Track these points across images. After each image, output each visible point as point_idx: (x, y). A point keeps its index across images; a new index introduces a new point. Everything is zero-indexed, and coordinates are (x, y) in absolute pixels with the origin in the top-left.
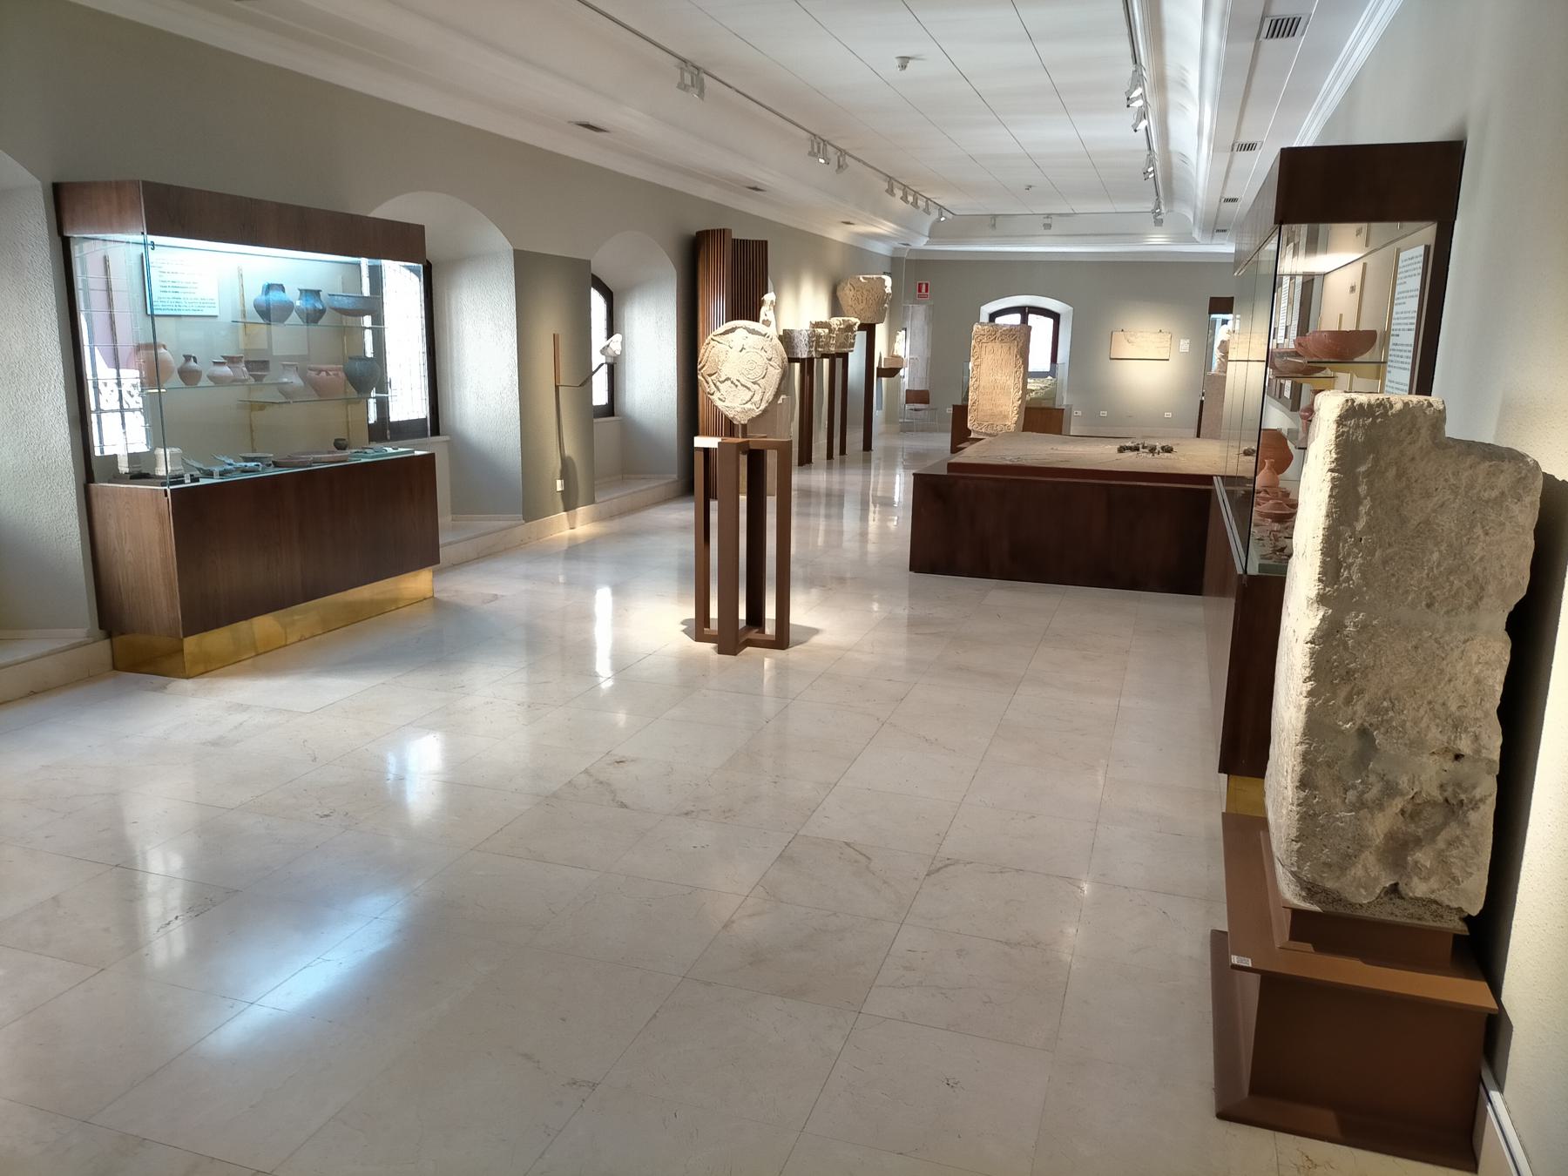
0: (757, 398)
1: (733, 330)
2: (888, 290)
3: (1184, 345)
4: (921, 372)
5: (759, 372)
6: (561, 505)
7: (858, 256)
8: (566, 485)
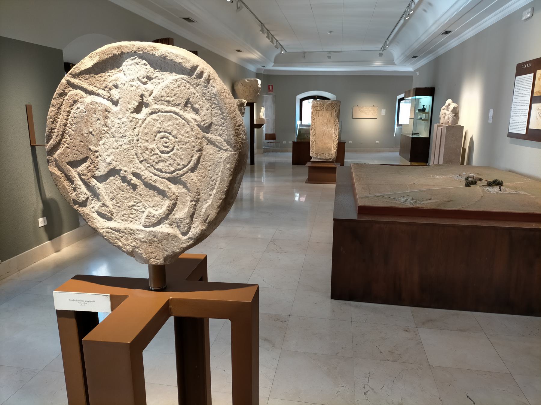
0: (181, 213)
1: (113, 62)
2: (259, 86)
3: (383, 112)
4: (271, 126)
5: (182, 157)
6: (44, 235)
7: (242, 71)
8: (49, 221)
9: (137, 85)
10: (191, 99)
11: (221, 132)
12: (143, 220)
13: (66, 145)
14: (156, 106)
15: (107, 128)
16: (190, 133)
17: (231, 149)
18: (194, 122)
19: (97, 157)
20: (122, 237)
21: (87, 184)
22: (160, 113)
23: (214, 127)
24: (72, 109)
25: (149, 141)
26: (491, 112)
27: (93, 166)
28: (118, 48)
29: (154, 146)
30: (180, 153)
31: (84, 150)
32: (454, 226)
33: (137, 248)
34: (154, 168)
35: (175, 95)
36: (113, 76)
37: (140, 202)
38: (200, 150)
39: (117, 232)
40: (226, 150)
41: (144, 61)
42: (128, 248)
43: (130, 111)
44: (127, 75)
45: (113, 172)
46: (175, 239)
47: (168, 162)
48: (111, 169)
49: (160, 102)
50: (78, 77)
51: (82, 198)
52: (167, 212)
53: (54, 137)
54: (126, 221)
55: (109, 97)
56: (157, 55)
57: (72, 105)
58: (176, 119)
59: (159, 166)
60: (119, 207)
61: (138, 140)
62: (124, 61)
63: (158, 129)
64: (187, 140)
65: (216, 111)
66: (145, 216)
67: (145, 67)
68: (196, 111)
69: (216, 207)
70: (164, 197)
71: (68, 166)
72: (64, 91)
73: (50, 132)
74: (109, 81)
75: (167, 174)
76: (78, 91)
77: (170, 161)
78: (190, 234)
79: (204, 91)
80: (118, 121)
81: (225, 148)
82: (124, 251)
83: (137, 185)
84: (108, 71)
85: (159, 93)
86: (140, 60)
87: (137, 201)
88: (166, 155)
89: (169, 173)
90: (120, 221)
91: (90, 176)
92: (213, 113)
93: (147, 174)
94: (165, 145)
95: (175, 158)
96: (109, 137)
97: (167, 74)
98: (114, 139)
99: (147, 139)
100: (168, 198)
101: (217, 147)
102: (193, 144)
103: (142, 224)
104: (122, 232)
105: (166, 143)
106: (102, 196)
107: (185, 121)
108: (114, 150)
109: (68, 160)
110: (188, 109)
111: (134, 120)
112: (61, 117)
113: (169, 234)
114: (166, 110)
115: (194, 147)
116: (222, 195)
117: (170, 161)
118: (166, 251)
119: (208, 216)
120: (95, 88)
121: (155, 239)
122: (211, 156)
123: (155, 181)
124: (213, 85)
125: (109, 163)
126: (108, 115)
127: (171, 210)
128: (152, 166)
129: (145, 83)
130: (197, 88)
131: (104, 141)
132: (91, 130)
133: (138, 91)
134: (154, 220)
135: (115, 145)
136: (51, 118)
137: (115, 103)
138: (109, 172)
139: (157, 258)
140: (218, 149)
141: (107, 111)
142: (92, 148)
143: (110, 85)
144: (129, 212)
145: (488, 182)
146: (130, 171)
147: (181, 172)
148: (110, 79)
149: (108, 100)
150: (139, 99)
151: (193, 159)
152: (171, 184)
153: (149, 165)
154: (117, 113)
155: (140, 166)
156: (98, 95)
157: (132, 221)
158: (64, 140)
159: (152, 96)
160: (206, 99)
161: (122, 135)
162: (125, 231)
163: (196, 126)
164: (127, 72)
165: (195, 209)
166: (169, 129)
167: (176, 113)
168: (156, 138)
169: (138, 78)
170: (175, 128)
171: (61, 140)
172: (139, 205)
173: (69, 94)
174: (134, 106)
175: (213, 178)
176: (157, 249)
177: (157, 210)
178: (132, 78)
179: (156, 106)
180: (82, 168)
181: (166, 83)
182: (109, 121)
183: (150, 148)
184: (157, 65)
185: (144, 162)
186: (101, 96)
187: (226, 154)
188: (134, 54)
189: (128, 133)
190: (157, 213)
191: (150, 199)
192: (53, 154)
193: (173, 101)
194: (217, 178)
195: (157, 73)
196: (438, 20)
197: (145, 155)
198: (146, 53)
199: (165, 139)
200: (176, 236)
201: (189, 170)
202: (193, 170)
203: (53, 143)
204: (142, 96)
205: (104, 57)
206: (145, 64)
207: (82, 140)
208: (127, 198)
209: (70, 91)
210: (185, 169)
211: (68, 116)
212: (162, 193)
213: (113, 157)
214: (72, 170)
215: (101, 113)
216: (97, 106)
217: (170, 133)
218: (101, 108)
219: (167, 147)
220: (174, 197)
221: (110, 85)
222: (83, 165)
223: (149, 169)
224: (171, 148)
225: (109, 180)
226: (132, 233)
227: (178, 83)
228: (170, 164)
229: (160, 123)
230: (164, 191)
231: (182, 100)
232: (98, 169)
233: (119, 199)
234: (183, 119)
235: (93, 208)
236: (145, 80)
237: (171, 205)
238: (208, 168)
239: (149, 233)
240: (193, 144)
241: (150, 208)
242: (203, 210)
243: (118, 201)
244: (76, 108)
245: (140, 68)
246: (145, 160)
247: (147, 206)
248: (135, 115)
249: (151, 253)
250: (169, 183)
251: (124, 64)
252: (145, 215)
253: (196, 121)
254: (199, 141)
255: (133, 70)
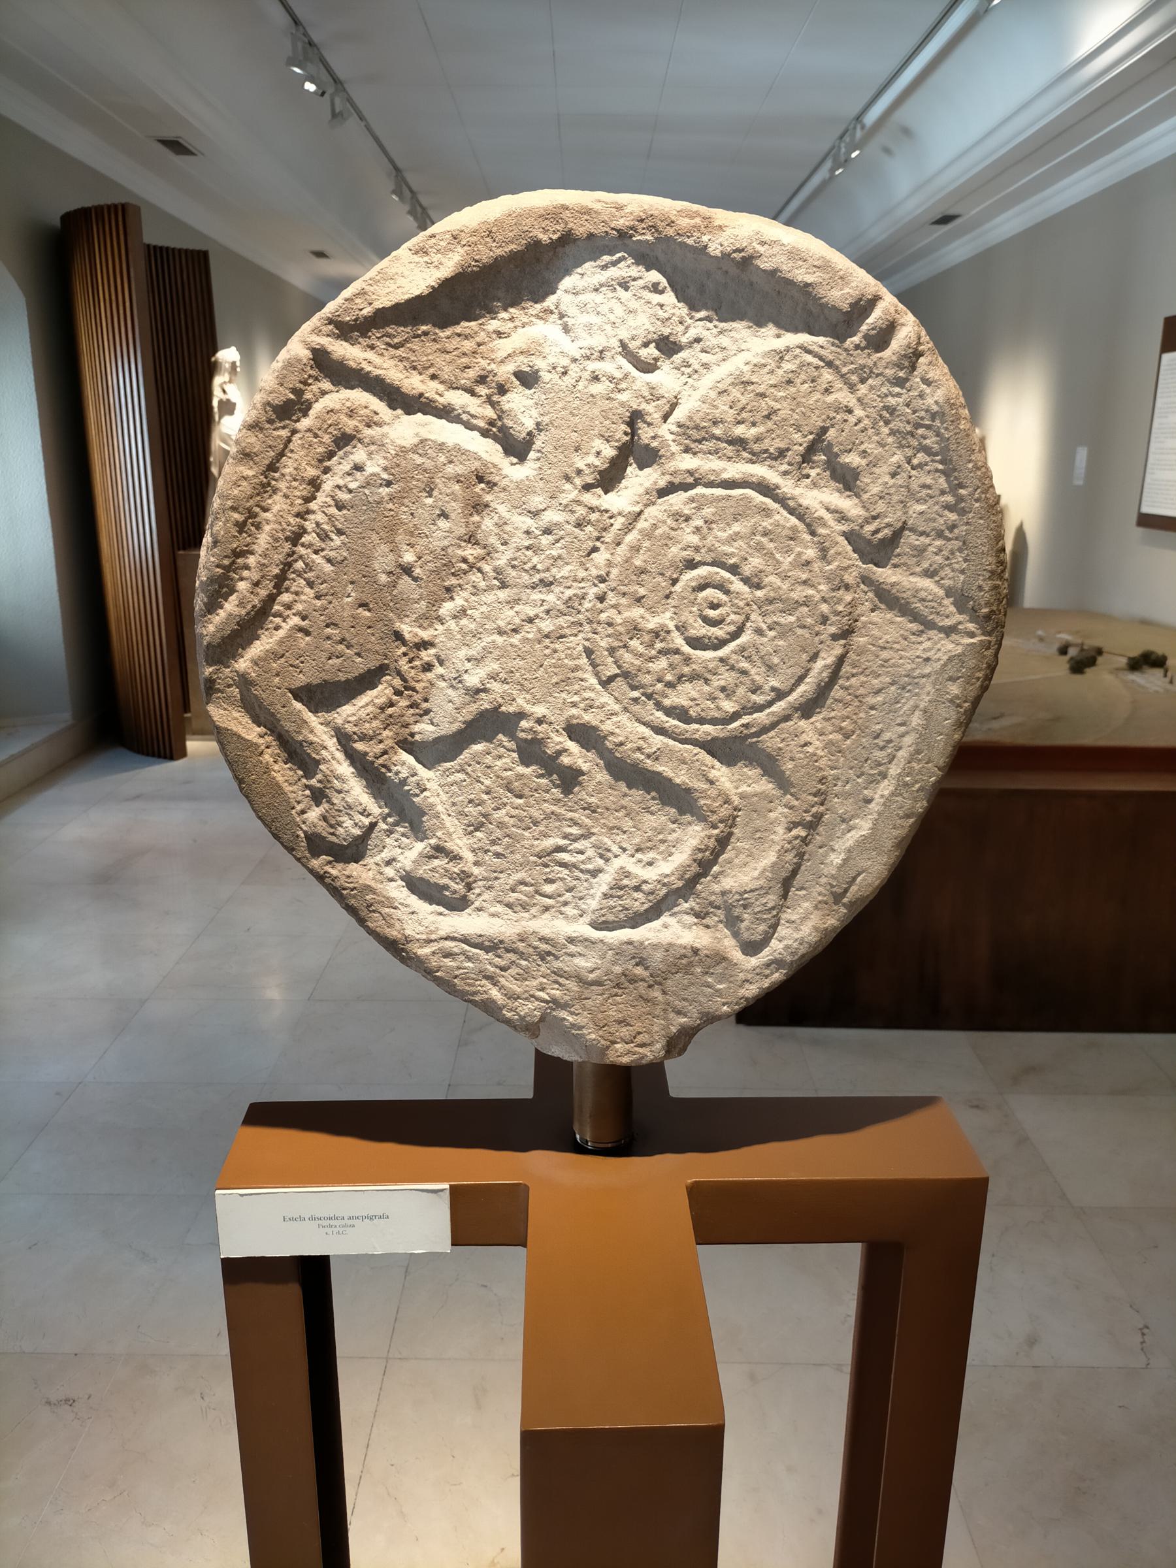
0: (744, 872)
1: (520, 274)
5: (769, 657)
9: (618, 375)
10: (832, 433)
11: (939, 559)
12: (593, 904)
13: (296, 620)
14: (688, 462)
15: (478, 551)
16: (816, 566)
17: (971, 626)
18: (832, 523)
19: (428, 667)
20: (503, 969)
21: (373, 775)
22: (700, 490)
23: (910, 538)
24: (326, 470)
25: (648, 602)
26: (1082, 454)
27: (404, 703)
28: (553, 214)
29: (666, 619)
30: (766, 643)
31: (372, 640)
32: (1091, 795)
33: (565, 1006)
34: (659, 706)
35: (768, 417)
36: (514, 334)
37: (587, 835)
38: (846, 633)
39: (487, 950)
40: (949, 631)
41: (654, 276)
42: (529, 1009)
43: (578, 481)
44: (580, 331)
45: (490, 724)
46: (718, 970)
47: (717, 682)
48: (483, 714)
49: (709, 445)
50: (364, 335)
51: (350, 827)
52: (695, 868)
53: (242, 586)
54: (525, 907)
55: (492, 423)
56: (714, 250)
57: (331, 455)
58: (766, 512)
59: (673, 699)
60: (498, 855)
61: (601, 599)
62: (568, 272)
63: (689, 553)
64: (799, 593)
65: (928, 480)
66: (605, 888)
67: (656, 298)
68: (846, 479)
69: (889, 844)
70: (682, 812)
71: (298, 706)
72: (298, 393)
73: (228, 569)
74: (502, 354)
75: (708, 728)
76: (359, 397)
77: (726, 678)
78: (776, 947)
79: (892, 401)
80: (528, 522)
81: (948, 622)
82: (507, 1021)
83: (581, 773)
84: (492, 313)
85: (705, 408)
86: (635, 271)
87: (575, 831)
88: (709, 654)
89: (713, 722)
90: (499, 908)
91: (390, 742)
92: (914, 486)
93: (627, 730)
94: (712, 613)
95: (745, 665)
96: (482, 584)
97: (740, 329)
98: (503, 595)
99: (642, 591)
100: (702, 818)
101: (915, 617)
102: (824, 608)
103: (587, 919)
104: (508, 951)
105: (714, 606)
106: (437, 816)
107: (801, 518)
108: (500, 640)
109: (301, 680)
110: (813, 473)
111: (594, 517)
112: (277, 503)
113: (696, 951)
114: (725, 476)
115: (824, 620)
116: (915, 800)
117: (726, 678)
118: (679, 1013)
119: (854, 879)
120: (434, 385)
121: (639, 971)
122: (885, 655)
123: (656, 757)
124: (930, 375)
125: (478, 691)
126: (488, 498)
127: (705, 864)
128: (649, 697)
129: (647, 367)
130: (863, 389)
131: (459, 601)
132: (409, 557)
133: (623, 397)
134: (639, 902)
135: (509, 615)
136: (234, 509)
137: (517, 448)
138: (469, 724)
139: (640, 1039)
140: (915, 627)
141: (480, 479)
142: (407, 629)
143: (505, 371)
144: (539, 872)
145: (1130, 659)
146: (559, 720)
147: (761, 717)
148: (503, 347)
149: (485, 433)
150: (620, 432)
151: (819, 664)
152: (717, 764)
153: (636, 694)
154: (525, 488)
155: (605, 698)
156: (446, 413)
157: (546, 909)
158: (286, 597)
159: (671, 420)
160: (892, 433)
161: (536, 578)
162: (521, 946)
163: (841, 539)
164: (578, 319)
165: (801, 855)
166: (733, 551)
167: (765, 489)
168: (678, 588)
169: (623, 345)
170: (759, 548)
171: (271, 599)
172: (578, 845)
173: (317, 408)
174: (597, 462)
175: (887, 736)
176: (642, 1008)
177: (650, 864)
178: (598, 341)
179: (688, 462)
180: (348, 713)
181: (737, 364)
182: (488, 523)
183: (650, 626)
184: (702, 290)
185: (620, 684)
186: (457, 420)
187: (950, 646)
188: (618, 242)
189: (566, 571)
190: (651, 874)
191: (628, 824)
192: (235, 656)
193: (758, 439)
194: (902, 736)
195: (699, 327)
196: (929, 180)
197: (628, 657)
198: (669, 239)
199: (709, 592)
200: (721, 958)
201: (796, 709)
202: (807, 709)
203: (238, 611)
204: (634, 418)
205: (487, 253)
206: (655, 288)
207: (366, 598)
208: (536, 823)
209: (324, 393)
210: (779, 707)
211: (308, 499)
212: (679, 800)
213: (495, 666)
214: (313, 719)
215: (457, 487)
216: (442, 459)
217: (734, 569)
218: (459, 469)
219: (714, 623)
220: (724, 812)
221: (505, 371)
222: (362, 700)
223: (636, 708)
224: (732, 628)
225: (465, 756)
226: (547, 951)
227: (787, 366)
228: (723, 689)
229: (698, 530)
230: (688, 791)
231: (797, 437)
232: (427, 712)
233: (501, 825)
234: (792, 512)
235: (389, 863)
236: (652, 351)
237: (712, 843)
238: (871, 700)
239: (619, 951)
240: (824, 608)
241: (624, 856)
242: (836, 859)
243: (498, 833)
244: (346, 466)
245: (634, 304)
246: (626, 675)
247: (615, 848)
248: (596, 498)
249: (620, 1022)
250: (709, 759)
251: (567, 283)
252: (603, 882)
253: (842, 517)
254: (848, 597)
255: (604, 309)
